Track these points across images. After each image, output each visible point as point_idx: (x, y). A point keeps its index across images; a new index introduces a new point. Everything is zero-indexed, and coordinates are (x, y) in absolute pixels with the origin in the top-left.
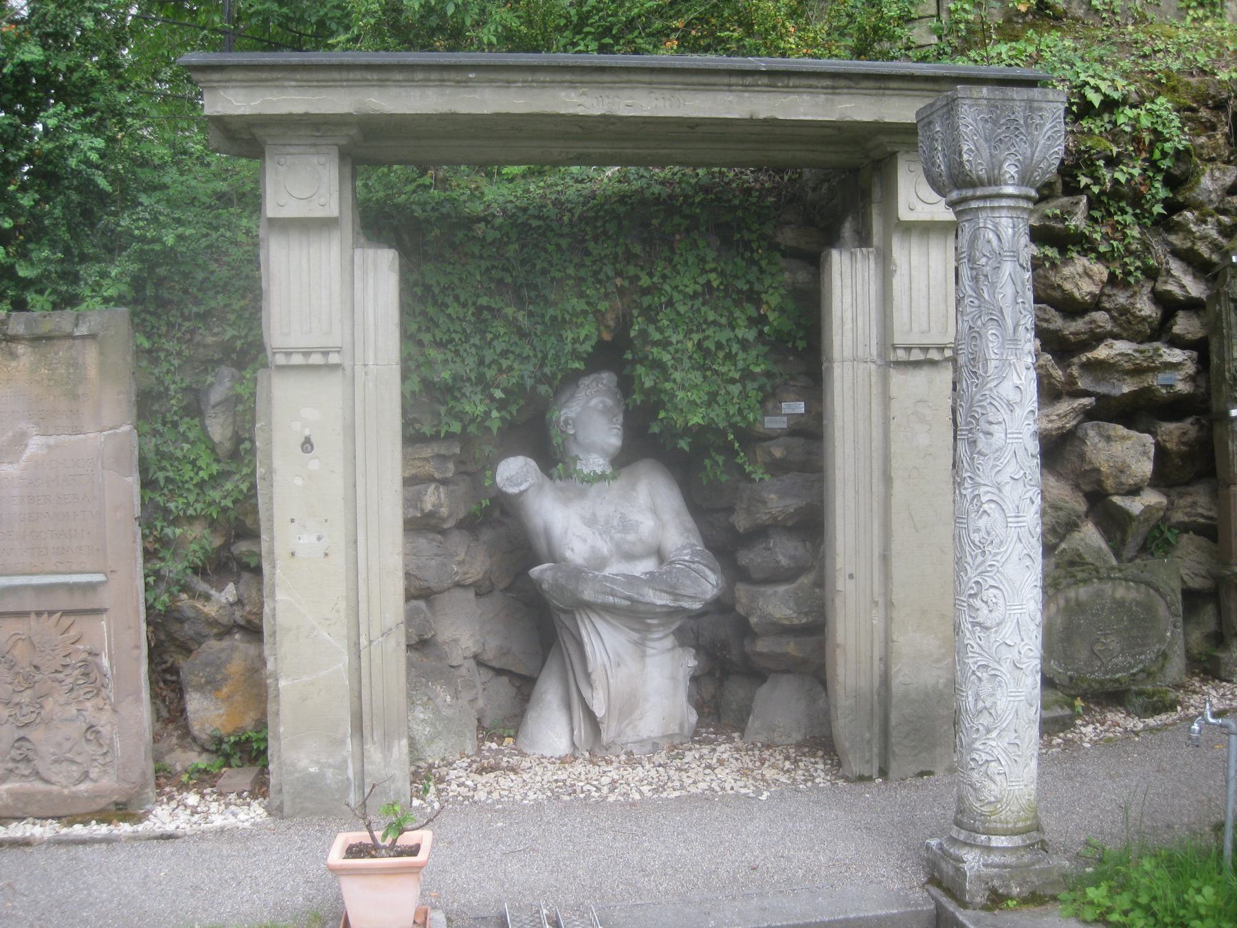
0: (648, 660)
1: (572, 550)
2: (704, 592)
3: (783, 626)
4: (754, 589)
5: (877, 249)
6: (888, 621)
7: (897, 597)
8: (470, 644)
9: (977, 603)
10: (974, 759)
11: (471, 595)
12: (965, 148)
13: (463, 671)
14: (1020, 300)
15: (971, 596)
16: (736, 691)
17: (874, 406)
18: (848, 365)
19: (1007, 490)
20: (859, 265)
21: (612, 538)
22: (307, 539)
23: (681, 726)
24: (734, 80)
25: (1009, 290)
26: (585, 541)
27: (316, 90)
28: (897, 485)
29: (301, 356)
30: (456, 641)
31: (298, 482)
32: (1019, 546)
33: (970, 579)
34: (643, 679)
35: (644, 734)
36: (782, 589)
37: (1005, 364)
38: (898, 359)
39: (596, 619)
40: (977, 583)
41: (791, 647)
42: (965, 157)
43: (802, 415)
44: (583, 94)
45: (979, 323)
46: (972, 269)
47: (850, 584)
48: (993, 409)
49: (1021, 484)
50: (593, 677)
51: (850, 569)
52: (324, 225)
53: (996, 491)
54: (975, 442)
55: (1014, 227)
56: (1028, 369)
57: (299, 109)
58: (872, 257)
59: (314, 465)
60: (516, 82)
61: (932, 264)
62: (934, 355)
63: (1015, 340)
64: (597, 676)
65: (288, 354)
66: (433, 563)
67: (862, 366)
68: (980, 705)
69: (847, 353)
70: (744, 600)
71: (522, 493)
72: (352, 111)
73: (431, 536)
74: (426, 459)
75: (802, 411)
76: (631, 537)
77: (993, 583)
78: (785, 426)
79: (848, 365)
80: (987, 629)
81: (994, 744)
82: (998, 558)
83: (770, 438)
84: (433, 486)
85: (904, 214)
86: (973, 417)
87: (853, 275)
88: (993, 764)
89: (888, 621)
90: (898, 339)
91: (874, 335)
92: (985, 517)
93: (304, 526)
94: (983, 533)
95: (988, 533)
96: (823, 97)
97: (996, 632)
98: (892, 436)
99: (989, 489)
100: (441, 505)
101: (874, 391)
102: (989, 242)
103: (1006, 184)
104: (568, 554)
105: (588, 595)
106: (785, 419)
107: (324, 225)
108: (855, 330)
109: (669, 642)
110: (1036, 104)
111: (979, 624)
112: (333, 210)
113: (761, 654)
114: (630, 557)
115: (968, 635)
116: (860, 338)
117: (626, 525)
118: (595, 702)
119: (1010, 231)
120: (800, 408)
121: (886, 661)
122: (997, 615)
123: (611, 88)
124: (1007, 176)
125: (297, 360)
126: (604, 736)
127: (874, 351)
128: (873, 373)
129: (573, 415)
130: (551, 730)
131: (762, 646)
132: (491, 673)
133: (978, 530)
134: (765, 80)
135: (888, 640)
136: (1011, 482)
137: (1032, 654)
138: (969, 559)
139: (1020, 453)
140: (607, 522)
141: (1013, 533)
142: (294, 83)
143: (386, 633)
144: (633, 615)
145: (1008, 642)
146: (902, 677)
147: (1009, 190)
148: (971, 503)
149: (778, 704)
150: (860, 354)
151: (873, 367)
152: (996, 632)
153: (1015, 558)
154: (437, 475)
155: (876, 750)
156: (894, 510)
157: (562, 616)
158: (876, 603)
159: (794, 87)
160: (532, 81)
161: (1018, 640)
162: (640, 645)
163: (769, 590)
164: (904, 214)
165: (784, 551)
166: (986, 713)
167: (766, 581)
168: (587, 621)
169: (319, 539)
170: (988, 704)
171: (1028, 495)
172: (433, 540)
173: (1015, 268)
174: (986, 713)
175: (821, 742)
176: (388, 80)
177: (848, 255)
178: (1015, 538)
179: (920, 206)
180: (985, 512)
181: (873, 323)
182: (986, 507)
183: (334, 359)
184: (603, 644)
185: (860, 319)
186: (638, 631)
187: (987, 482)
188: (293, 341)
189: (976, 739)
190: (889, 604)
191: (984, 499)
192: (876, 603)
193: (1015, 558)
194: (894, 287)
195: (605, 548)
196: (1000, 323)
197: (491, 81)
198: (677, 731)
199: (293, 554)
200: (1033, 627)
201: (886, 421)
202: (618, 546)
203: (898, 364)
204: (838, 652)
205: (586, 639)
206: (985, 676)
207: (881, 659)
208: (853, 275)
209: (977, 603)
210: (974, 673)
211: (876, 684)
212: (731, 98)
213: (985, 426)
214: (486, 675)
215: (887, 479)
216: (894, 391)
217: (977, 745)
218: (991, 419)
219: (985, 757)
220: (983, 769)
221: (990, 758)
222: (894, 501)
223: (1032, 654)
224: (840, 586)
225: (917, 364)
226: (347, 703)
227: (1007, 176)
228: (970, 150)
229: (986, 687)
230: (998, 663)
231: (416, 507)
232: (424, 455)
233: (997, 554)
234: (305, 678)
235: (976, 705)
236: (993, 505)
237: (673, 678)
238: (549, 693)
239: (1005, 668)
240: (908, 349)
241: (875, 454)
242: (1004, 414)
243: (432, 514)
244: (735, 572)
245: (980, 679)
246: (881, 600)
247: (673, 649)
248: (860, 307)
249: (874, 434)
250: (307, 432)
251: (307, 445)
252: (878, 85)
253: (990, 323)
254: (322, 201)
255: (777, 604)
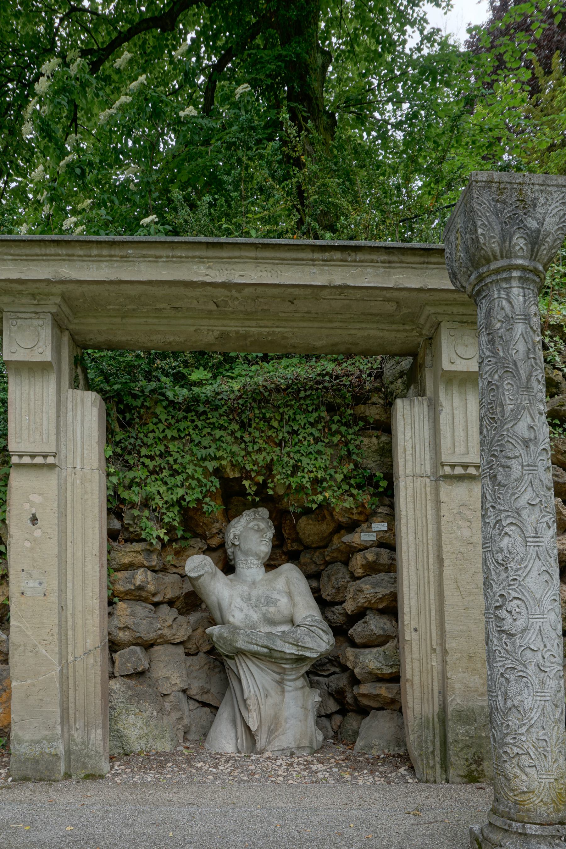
0: (286, 694)
1: (233, 616)
2: (319, 646)
3: (376, 674)
4: (358, 650)
5: (430, 400)
6: (444, 662)
7: (450, 644)
8: (178, 681)
9: (503, 613)
10: (506, 752)
11: (181, 650)
12: (479, 223)
13: (171, 698)
14: (532, 356)
15: (497, 608)
16: (352, 721)
17: (429, 509)
18: (409, 479)
19: (525, 513)
20: (416, 409)
21: (260, 610)
22: (33, 584)
23: (311, 741)
24: (316, 255)
25: (521, 347)
26: (242, 611)
27: (26, 263)
28: (447, 563)
29: (29, 458)
30: (167, 678)
31: (27, 544)
32: (538, 562)
33: (495, 593)
34: (284, 709)
35: (285, 745)
36: (374, 650)
37: (519, 408)
38: (448, 475)
39: (250, 664)
40: (502, 596)
41: (383, 690)
42: (480, 231)
43: (386, 531)
44: (209, 267)
45: (496, 377)
46: (488, 334)
47: (415, 636)
48: (510, 446)
49: (537, 509)
50: (248, 702)
51: (414, 624)
52: (41, 368)
53: (516, 516)
54: (495, 476)
55: (524, 296)
56: (541, 414)
57: (14, 276)
58: (425, 403)
59: (38, 533)
60: (161, 257)
61: (469, 405)
62: (472, 471)
63: (528, 388)
64: (251, 702)
65: (21, 456)
66: (145, 621)
67: (419, 479)
68: (509, 703)
69: (409, 471)
70: (351, 658)
71: (199, 577)
72: (50, 278)
73: (144, 604)
74: (138, 552)
75: (386, 529)
76: (272, 609)
77: (516, 595)
78: (375, 539)
79: (409, 479)
80: (513, 635)
81: (523, 738)
82: (519, 573)
83: (366, 548)
84: (142, 569)
85: (446, 366)
86: (493, 455)
87: (412, 416)
88: (524, 757)
89: (444, 662)
90: (445, 458)
91: (428, 457)
92: (506, 539)
93: (31, 575)
94: (506, 553)
95: (510, 552)
96: (382, 270)
97: (521, 638)
98: (443, 529)
99: (510, 514)
100: (148, 583)
101: (429, 497)
102: (503, 309)
103: (517, 257)
104: (231, 619)
105: (241, 644)
106: (374, 534)
107: (41, 368)
108: (413, 454)
109: (300, 683)
110: (534, 46)
111: (504, 631)
112: (48, 356)
113: (364, 695)
114: (272, 622)
115: (495, 641)
116: (418, 460)
117: (269, 601)
118: (250, 720)
119: (521, 298)
120: (384, 526)
121: (443, 693)
122: (520, 624)
123: (229, 263)
124: (517, 248)
125: (26, 460)
126: (258, 744)
127: (428, 469)
128: (428, 484)
129: (238, 532)
130: (225, 738)
131: (364, 689)
132: (197, 705)
133: (501, 551)
134: (338, 255)
135: (444, 677)
136: (529, 507)
137: (555, 660)
138: (494, 577)
139: (537, 483)
140: (258, 600)
141: (532, 552)
142: (10, 257)
143: (87, 653)
144: (270, 658)
145: (532, 647)
146: (456, 701)
147: (520, 261)
148: (494, 528)
149: (375, 731)
150: (418, 471)
151: (428, 480)
152: (521, 638)
153: (534, 573)
154: (146, 563)
155: (438, 759)
156: (445, 582)
157: (229, 661)
158: (435, 650)
159: (360, 261)
160: (173, 257)
161: (542, 647)
162: (280, 683)
163: (367, 651)
164: (446, 366)
165: (375, 624)
166: (514, 710)
167: (366, 646)
168: (243, 665)
169: (40, 584)
170: (516, 703)
171: (545, 519)
172: (145, 607)
173: (526, 328)
174: (514, 710)
175: (402, 757)
176: (73, 255)
177: (408, 402)
178: (534, 556)
179: (458, 361)
180: (506, 534)
181: (427, 449)
182: (506, 529)
183: (50, 460)
184: (254, 680)
185: (417, 447)
186: (279, 674)
187: (507, 508)
188: (22, 448)
189: (507, 734)
190: (445, 652)
191: (504, 523)
192: (435, 650)
193: (534, 573)
194: (441, 421)
195: (255, 616)
196: (516, 375)
197: (144, 256)
198: (308, 744)
199: (23, 594)
200: (554, 635)
201: (438, 522)
202: (264, 615)
203: (446, 477)
204: (408, 685)
205: (243, 677)
206: (512, 677)
207: (440, 692)
208: (412, 416)
209: (503, 613)
210: (502, 675)
211: (437, 710)
212: (315, 271)
213: (505, 461)
214: (193, 705)
215: (440, 561)
216: (443, 497)
217: (509, 739)
218: (509, 454)
219: (516, 750)
220: (515, 761)
221: (521, 752)
222: (445, 575)
223: (555, 660)
224: (407, 637)
225: (460, 478)
226: (58, 700)
227: (517, 248)
228: (483, 224)
229: (514, 687)
230: (525, 666)
231: (130, 583)
232: (137, 549)
233: (518, 570)
234: (29, 681)
235: (505, 704)
236: (513, 528)
237: (304, 708)
238: (224, 714)
239: (531, 669)
240: (453, 466)
241: (430, 542)
242: (520, 450)
243: (140, 588)
244: (340, 631)
245: (508, 680)
246: (438, 649)
247: (303, 687)
248: (417, 437)
249: (430, 528)
250: (34, 511)
251: (34, 520)
252: (422, 259)
253: (505, 375)
254: (41, 350)
255: (370, 660)
